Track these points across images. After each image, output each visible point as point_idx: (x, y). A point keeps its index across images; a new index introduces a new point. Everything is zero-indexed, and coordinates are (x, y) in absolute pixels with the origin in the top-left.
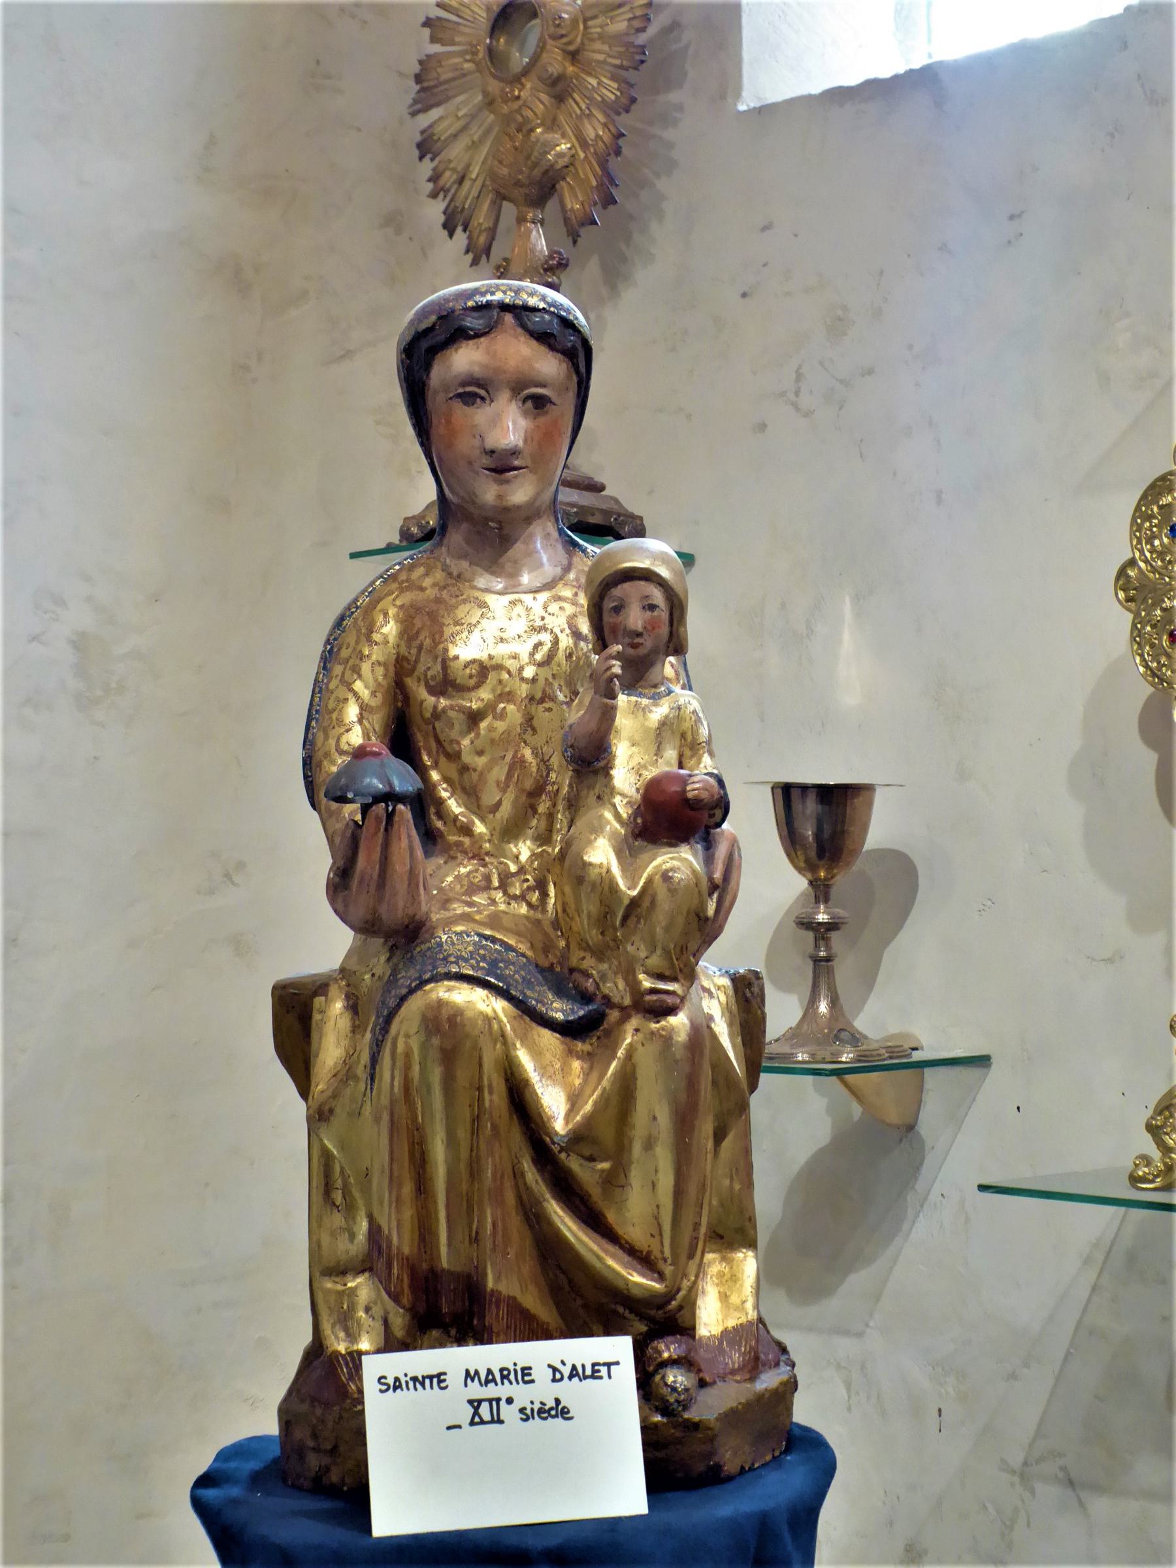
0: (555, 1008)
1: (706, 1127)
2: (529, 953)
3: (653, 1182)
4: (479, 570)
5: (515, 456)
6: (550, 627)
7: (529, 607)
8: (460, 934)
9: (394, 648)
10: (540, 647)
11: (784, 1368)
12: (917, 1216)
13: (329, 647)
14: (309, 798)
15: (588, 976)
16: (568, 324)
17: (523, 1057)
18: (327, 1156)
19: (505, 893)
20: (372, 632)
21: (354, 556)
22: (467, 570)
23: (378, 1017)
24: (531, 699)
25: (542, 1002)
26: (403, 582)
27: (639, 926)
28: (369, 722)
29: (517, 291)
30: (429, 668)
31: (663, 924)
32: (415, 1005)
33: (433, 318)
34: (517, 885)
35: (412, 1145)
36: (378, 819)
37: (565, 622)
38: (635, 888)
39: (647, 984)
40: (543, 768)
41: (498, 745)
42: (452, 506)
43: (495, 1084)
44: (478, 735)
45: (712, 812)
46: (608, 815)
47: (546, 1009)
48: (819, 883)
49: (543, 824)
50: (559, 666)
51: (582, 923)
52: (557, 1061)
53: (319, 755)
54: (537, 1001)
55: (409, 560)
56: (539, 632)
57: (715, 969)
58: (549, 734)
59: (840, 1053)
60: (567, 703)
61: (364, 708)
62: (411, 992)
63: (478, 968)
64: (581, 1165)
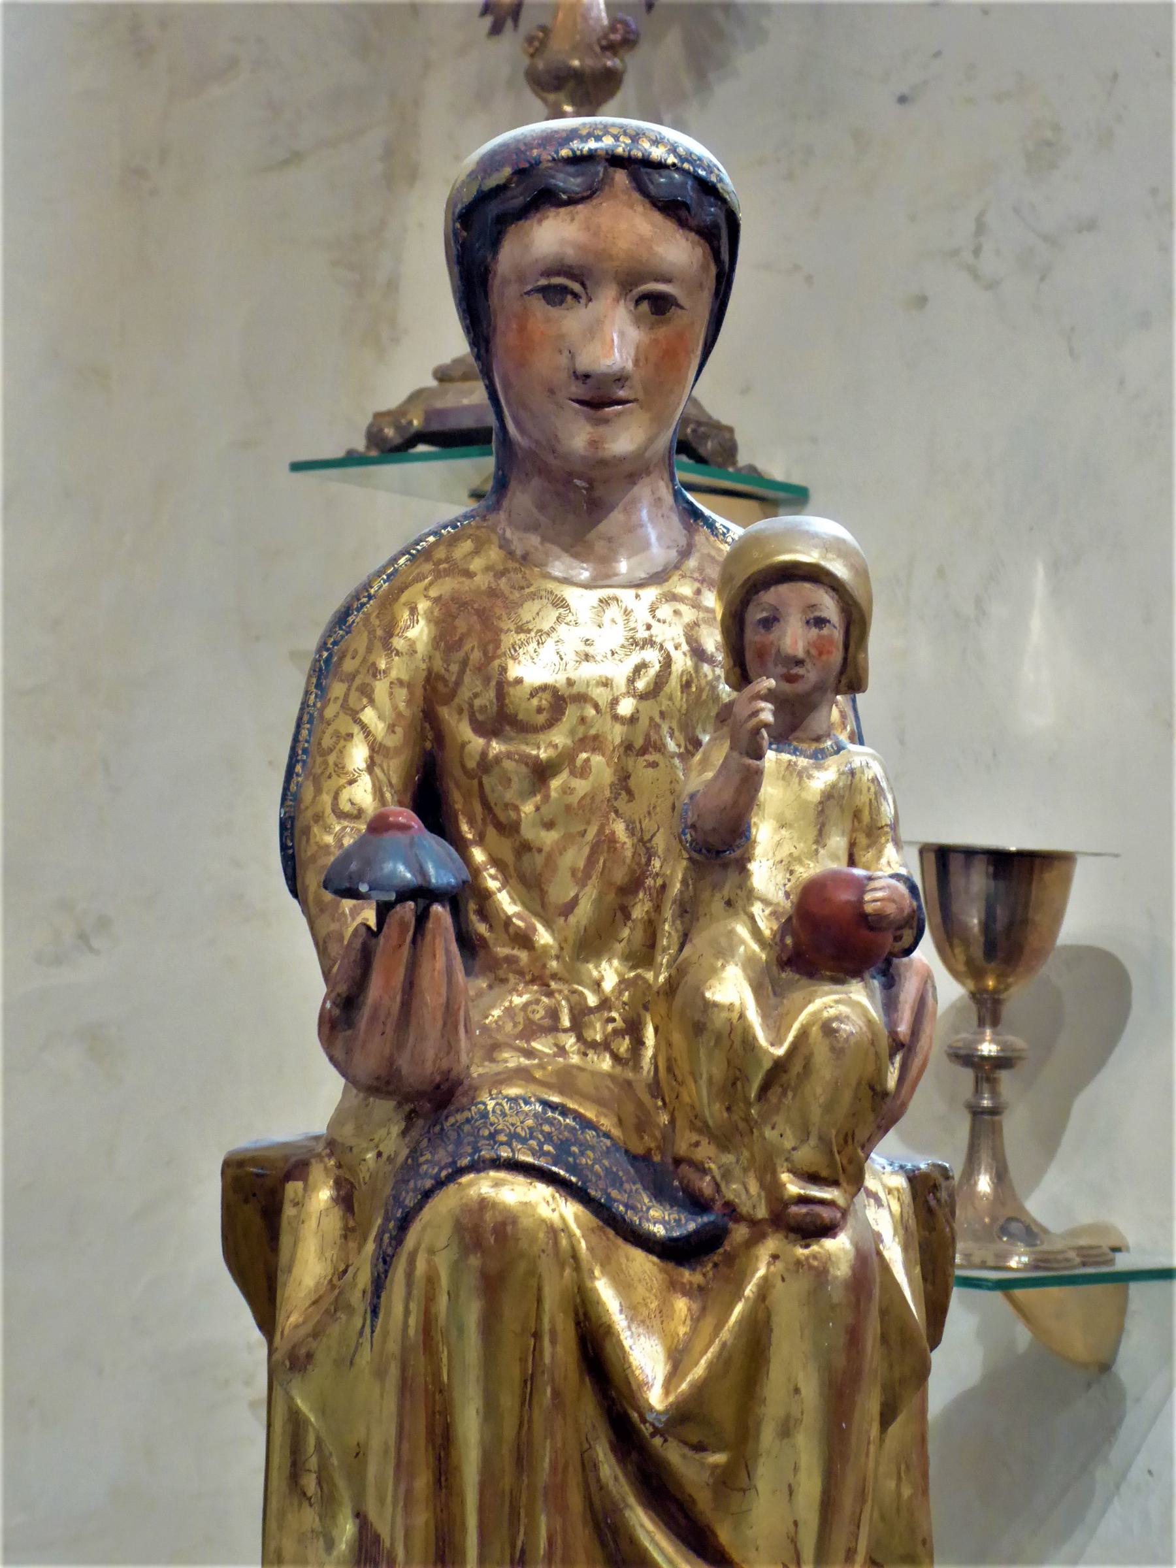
0: (653, 1217)
1: (870, 1403)
2: (616, 1132)
3: (790, 1486)
4: (556, 550)
5: (620, 384)
6: (658, 640)
7: (629, 609)
8: (513, 1100)
9: (424, 661)
10: (643, 671)
12: (1109, 1501)
13: (325, 654)
14: (287, 879)
15: (704, 1171)
16: (708, 189)
17: (606, 1292)
18: (296, 1421)
19: (580, 1038)
20: (391, 636)
21: (297, 467)
22: (536, 549)
23: (387, 1219)
24: (628, 747)
25: (633, 1208)
26: (440, 562)
27: (784, 1100)
28: (383, 771)
29: (636, 137)
30: (476, 695)
31: (822, 1100)
32: (445, 1203)
33: (507, 171)
34: (598, 1026)
35: (431, 1415)
36: (403, 925)
37: (682, 633)
38: (781, 1044)
39: (793, 1188)
40: (642, 851)
41: (576, 814)
42: (519, 452)
43: (560, 1327)
44: (547, 798)
45: (899, 933)
46: (742, 931)
47: (640, 1219)
48: (985, 996)
49: (639, 935)
51: (699, 1092)
52: (653, 1298)
53: (306, 817)
54: (627, 1206)
55: (449, 529)
56: (642, 648)
57: (884, 1161)
58: (654, 800)
59: (1006, 1256)
60: (680, 756)
61: (376, 750)
62: (440, 1184)
63: (542, 1153)
64: (684, 1456)
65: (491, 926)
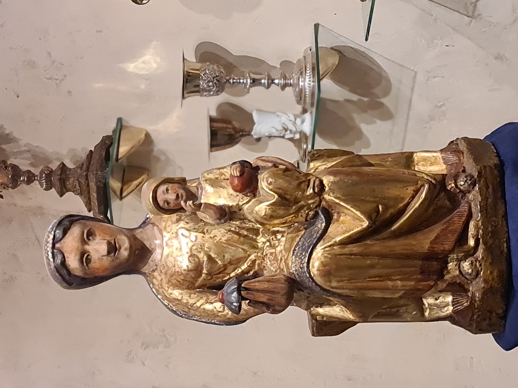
11: (458, 142)
13: (184, 316)
20: (178, 299)
23: (324, 294)
32: (319, 280)
45: (246, 167)
46: (246, 207)
47: (321, 230)
50: (191, 227)
56: (178, 235)
62: (314, 281)
65: (250, 271)
